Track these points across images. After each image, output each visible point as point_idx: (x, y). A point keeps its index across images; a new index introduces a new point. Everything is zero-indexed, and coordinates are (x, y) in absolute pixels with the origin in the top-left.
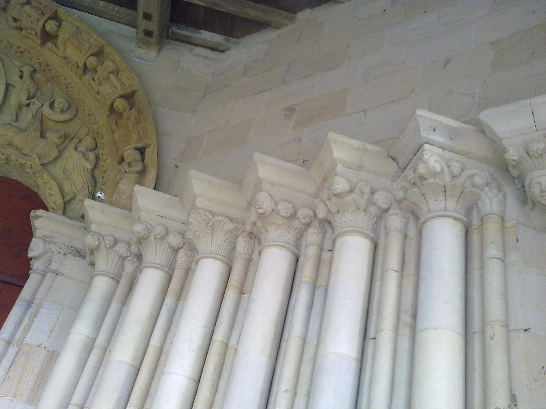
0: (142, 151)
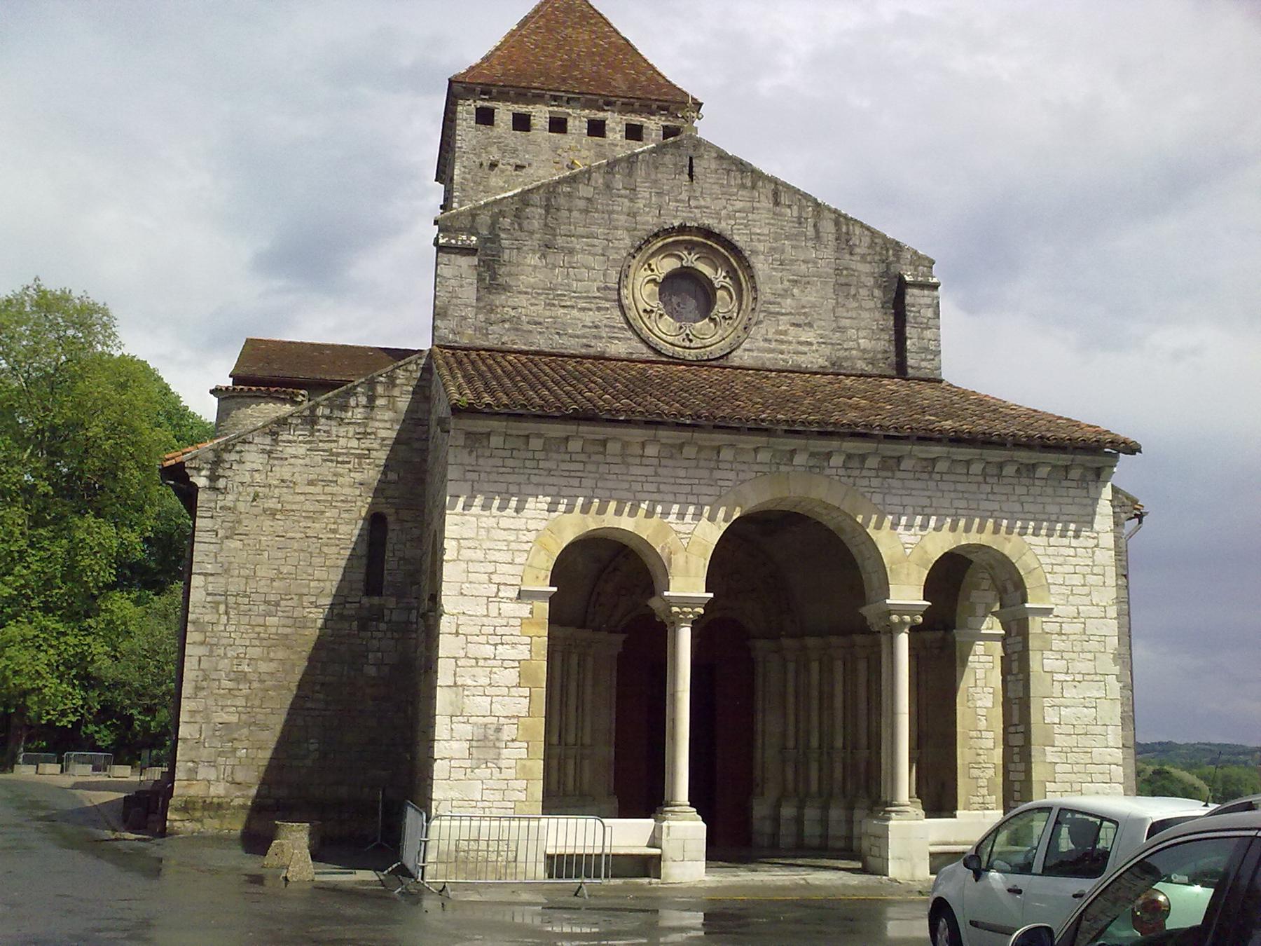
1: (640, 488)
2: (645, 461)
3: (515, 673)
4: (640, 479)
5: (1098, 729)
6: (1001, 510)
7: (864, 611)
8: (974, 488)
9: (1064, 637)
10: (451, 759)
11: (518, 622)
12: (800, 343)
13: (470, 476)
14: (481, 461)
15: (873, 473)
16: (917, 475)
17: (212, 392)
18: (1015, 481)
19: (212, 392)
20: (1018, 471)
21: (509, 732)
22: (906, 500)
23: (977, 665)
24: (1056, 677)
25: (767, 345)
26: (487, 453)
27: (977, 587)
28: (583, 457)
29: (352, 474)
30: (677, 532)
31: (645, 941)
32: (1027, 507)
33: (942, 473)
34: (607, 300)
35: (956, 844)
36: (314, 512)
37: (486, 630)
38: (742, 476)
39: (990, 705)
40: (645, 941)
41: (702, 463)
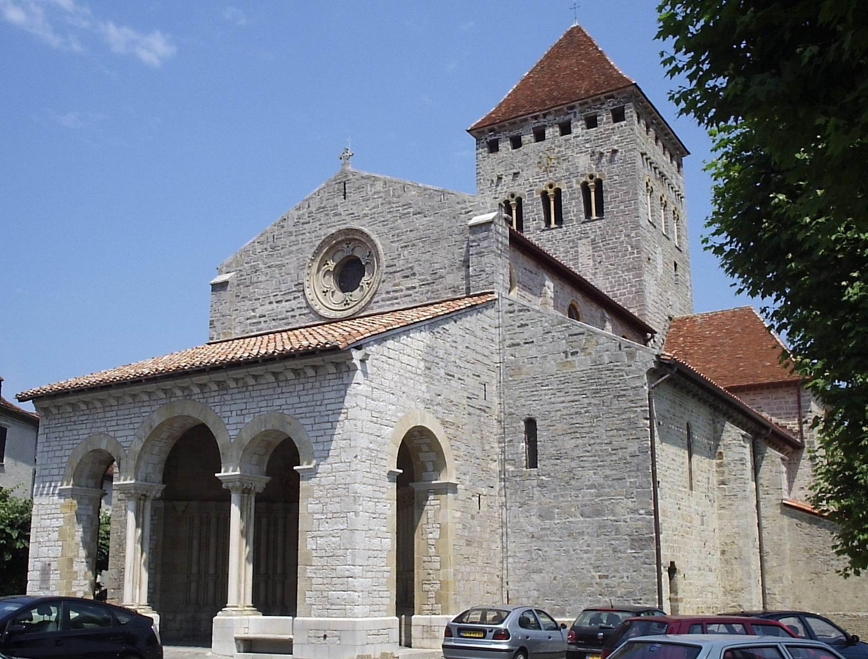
5: (341, 552)
8: (271, 391)
9: (322, 488)
12: (408, 289)
15: (216, 393)
18: (296, 382)
21: (54, 565)
22: (234, 407)
24: (316, 516)
35: (400, 636)
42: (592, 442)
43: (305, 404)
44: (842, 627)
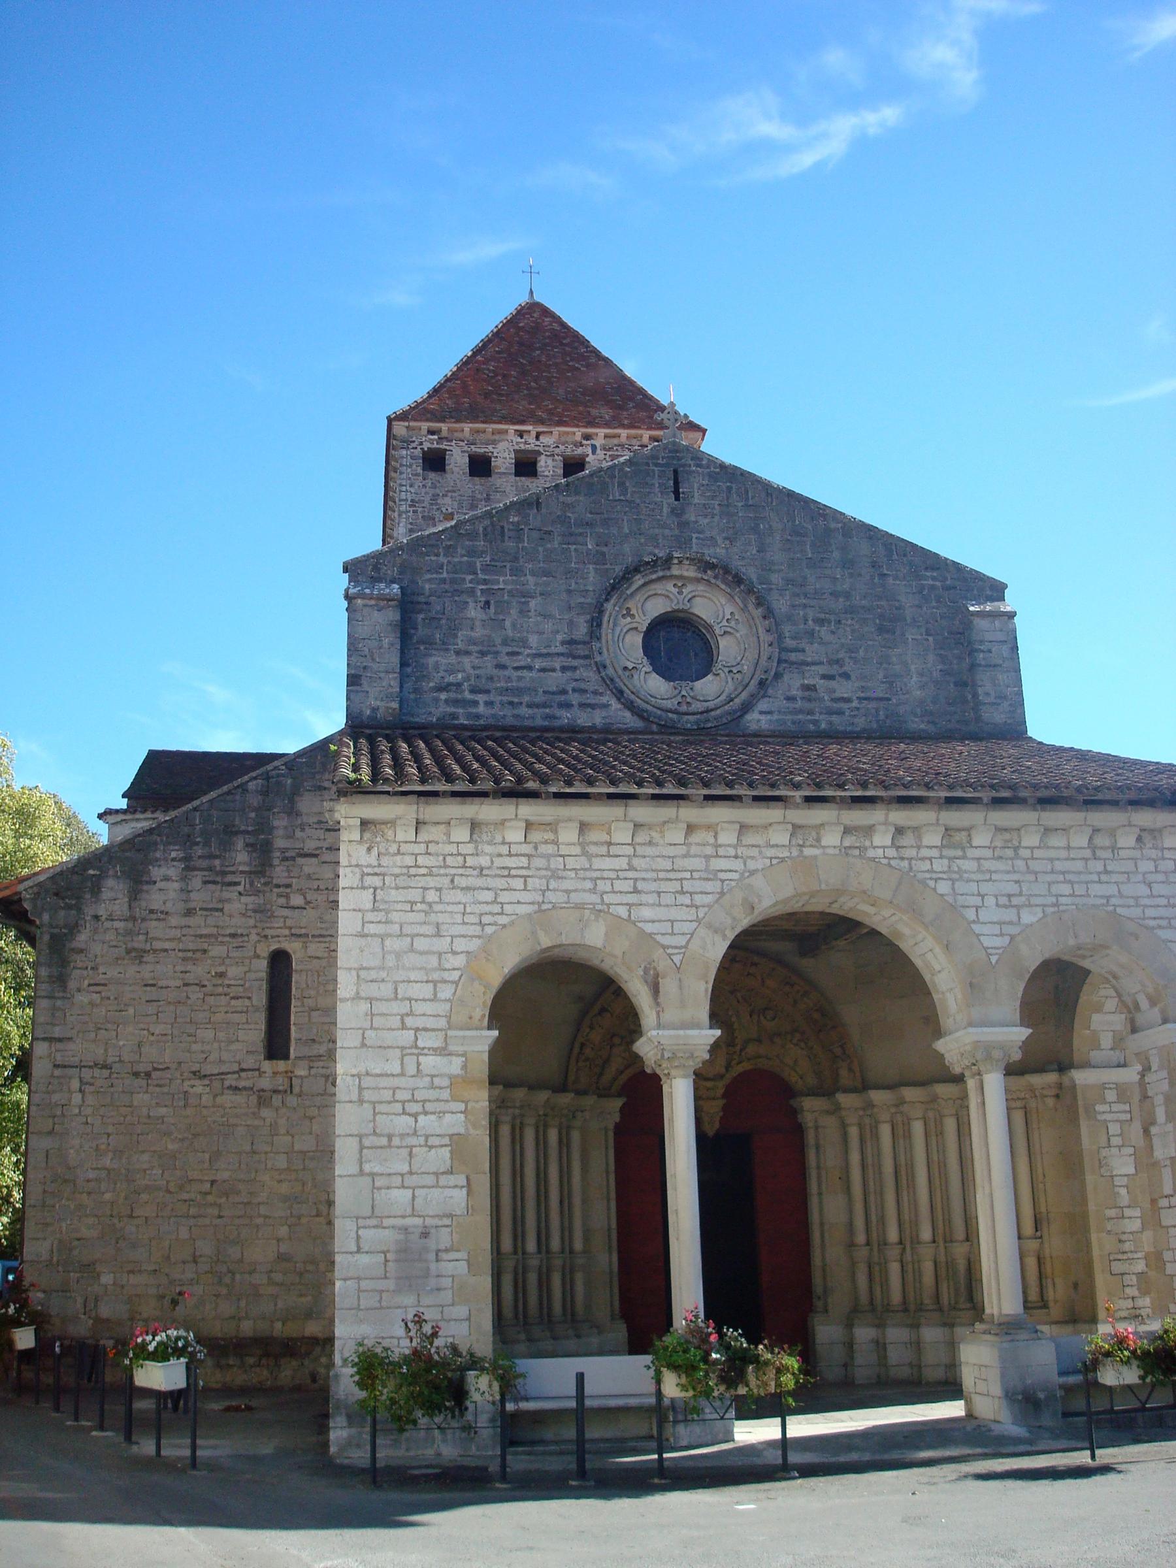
0: (841, 1046)
1: (609, 888)
2: (614, 850)
3: (446, 1153)
4: (606, 874)
6: (1121, 895)
7: (940, 1045)
10: (359, 1279)
11: (445, 1082)
13: (369, 881)
14: (385, 861)
16: (998, 853)
17: (100, 816)
19: (100, 816)
20: (1139, 839)
21: (444, 1238)
23: (1108, 1117)
25: (791, 705)
26: (393, 848)
27: (1099, 1009)
28: (527, 849)
29: (243, 899)
30: (664, 947)
31: (752, 1506)
32: (1158, 889)
33: (1032, 848)
34: (574, 657)
36: (194, 951)
37: (400, 1095)
38: (752, 865)
39: (1132, 1171)
40: (752, 1506)
41: (694, 850)
42: (383, 974)
43: (1164, 901)
44: (399, 1062)
